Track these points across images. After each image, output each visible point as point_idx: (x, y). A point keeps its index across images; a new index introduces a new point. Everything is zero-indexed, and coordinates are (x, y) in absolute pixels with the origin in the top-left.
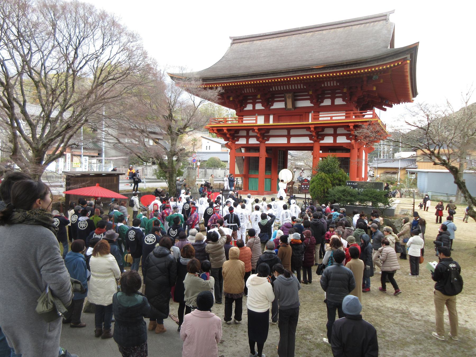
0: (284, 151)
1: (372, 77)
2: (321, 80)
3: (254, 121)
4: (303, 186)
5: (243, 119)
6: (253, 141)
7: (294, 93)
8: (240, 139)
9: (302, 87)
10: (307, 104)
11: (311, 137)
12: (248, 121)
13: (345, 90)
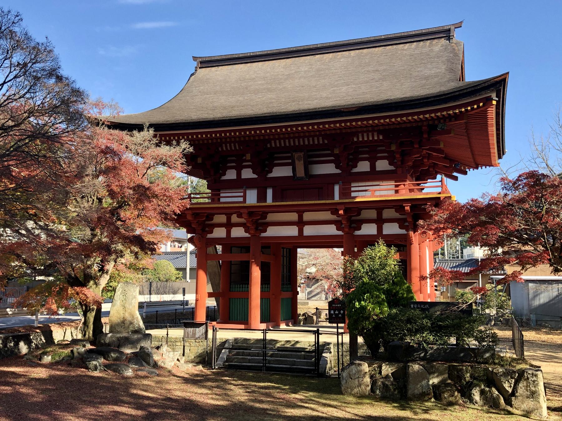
0: (290, 249)
1: (437, 126)
2: (354, 130)
3: (241, 199)
4: (332, 312)
5: (219, 195)
6: (238, 232)
9: (321, 142)
10: (329, 169)
13: (393, 148)
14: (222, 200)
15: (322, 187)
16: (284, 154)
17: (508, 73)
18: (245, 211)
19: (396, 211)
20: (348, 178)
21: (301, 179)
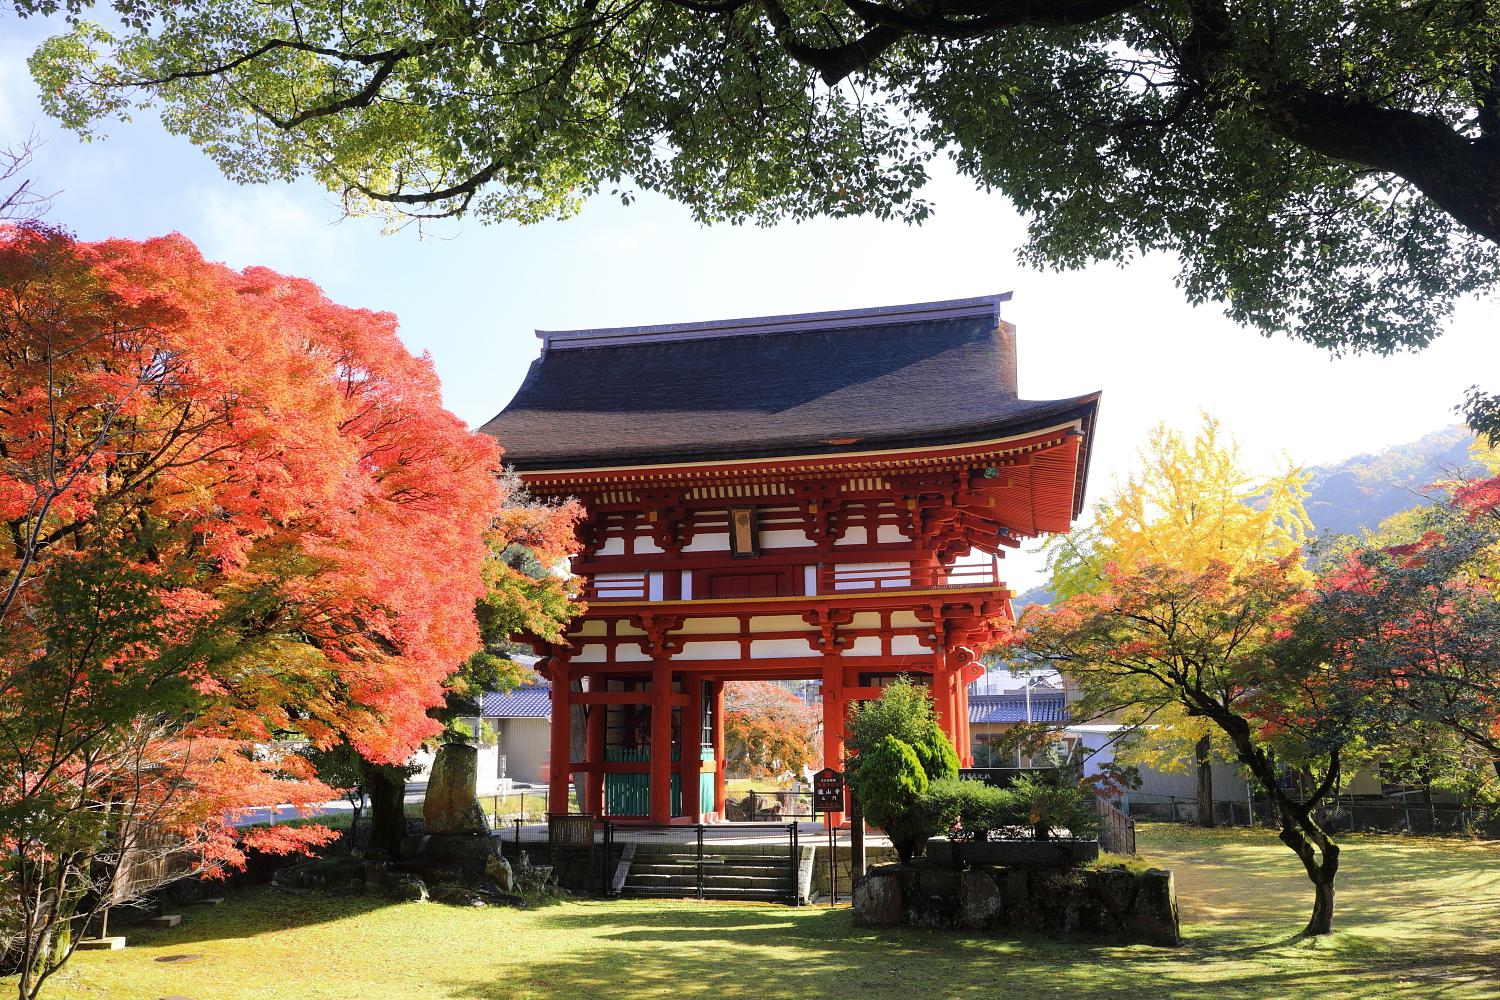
3: (640, 593)
4: (821, 792)
6: (629, 653)
8: (859, 641)
10: (796, 539)
11: (813, 638)
12: (616, 588)
13: (813, 509)
14: (601, 594)
15: (782, 573)
16: (721, 512)
18: (649, 614)
19: (805, 619)
20: (828, 556)
21: (746, 556)
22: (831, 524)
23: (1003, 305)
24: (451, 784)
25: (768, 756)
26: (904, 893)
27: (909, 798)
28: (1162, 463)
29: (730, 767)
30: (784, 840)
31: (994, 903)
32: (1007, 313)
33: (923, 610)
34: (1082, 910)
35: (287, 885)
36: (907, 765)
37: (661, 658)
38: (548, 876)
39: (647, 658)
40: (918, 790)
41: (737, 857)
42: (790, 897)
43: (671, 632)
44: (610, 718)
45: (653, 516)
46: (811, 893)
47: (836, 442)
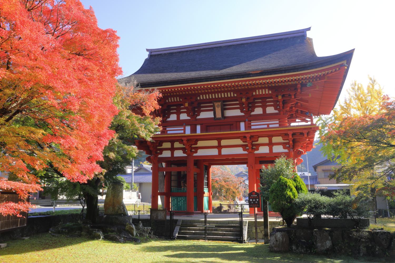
6: (179, 154)
7: (224, 101)
9: (178, 100)
10: (237, 113)
11: (244, 147)
12: (173, 131)
14: (169, 132)
15: (233, 123)
17: (354, 49)
20: (249, 118)
21: (219, 119)
22: (249, 107)
23: (308, 32)
24: (114, 197)
25: (230, 187)
26: (290, 239)
27: (290, 200)
28: (356, 95)
29: (214, 195)
30: (238, 219)
31: (328, 244)
32: (309, 34)
33: (285, 135)
34: (367, 247)
35: (54, 233)
36: (289, 187)
37: (190, 155)
38: (149, 231)
39: (185, 155)
40: (294, 197)
41: (220, 225)
42: (241, 241)
43: (193, 146)
44: (173, 178)
45: (187, 105)
46: (247, 238)
47: (253, 73)
